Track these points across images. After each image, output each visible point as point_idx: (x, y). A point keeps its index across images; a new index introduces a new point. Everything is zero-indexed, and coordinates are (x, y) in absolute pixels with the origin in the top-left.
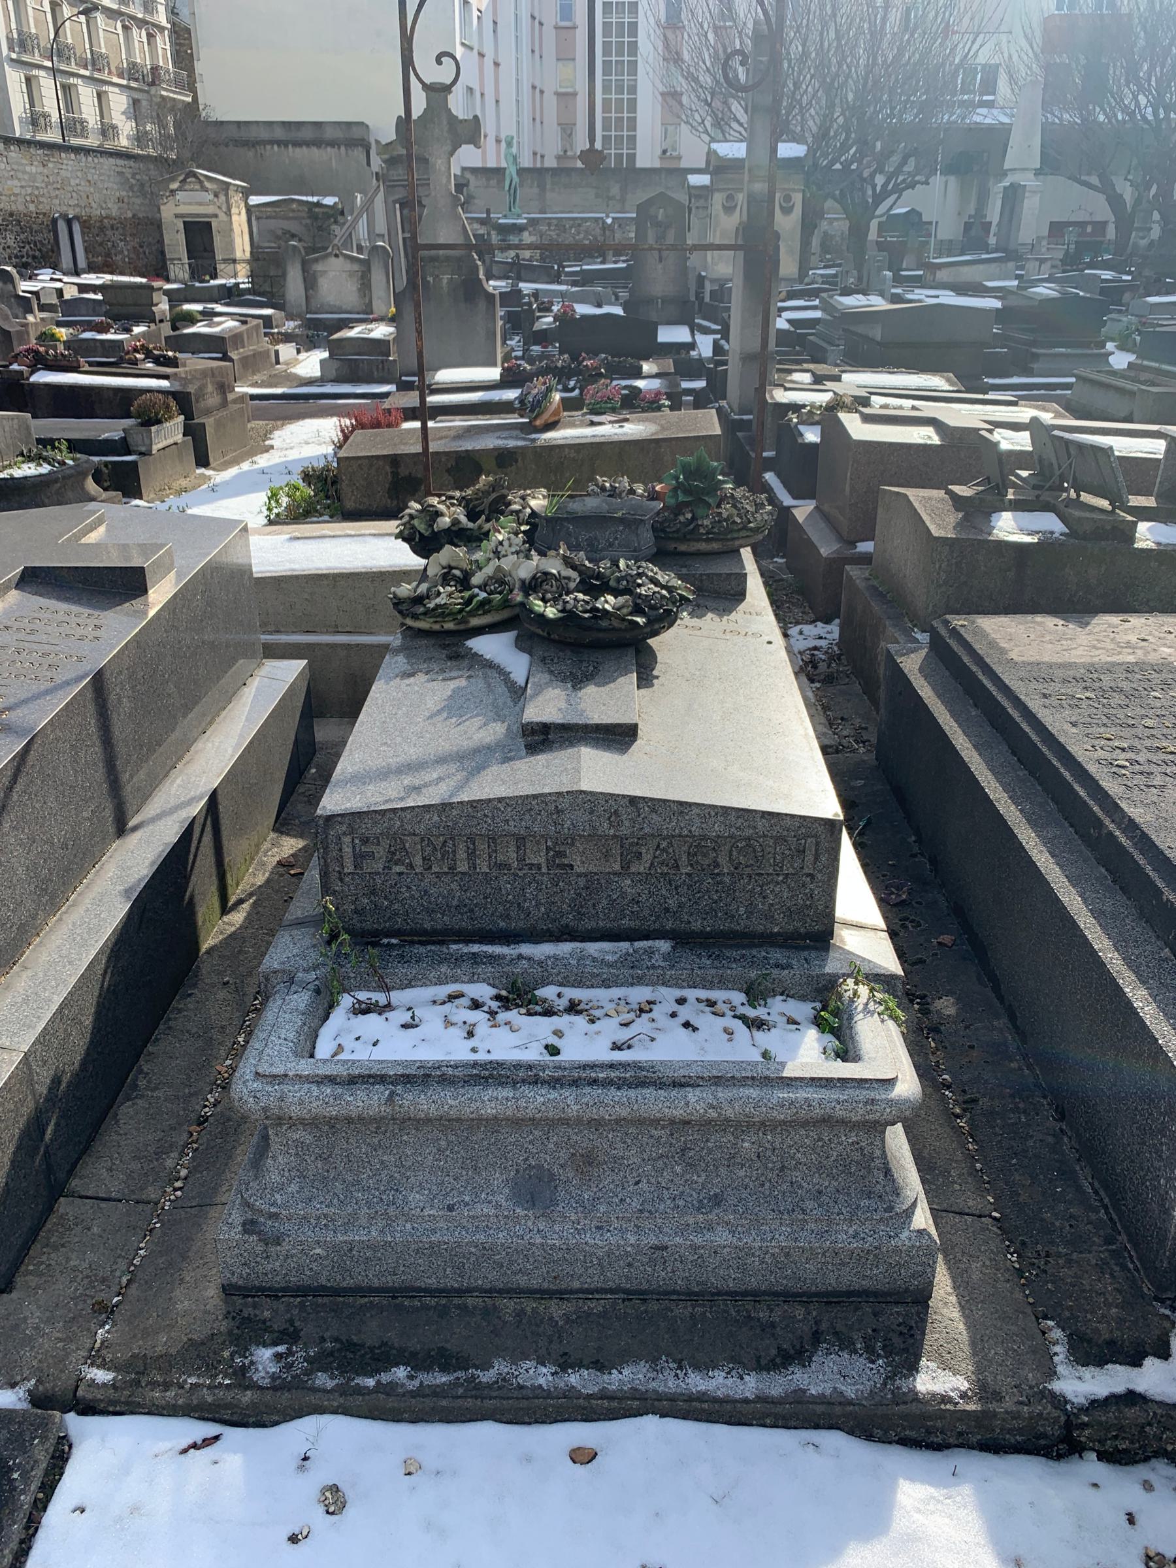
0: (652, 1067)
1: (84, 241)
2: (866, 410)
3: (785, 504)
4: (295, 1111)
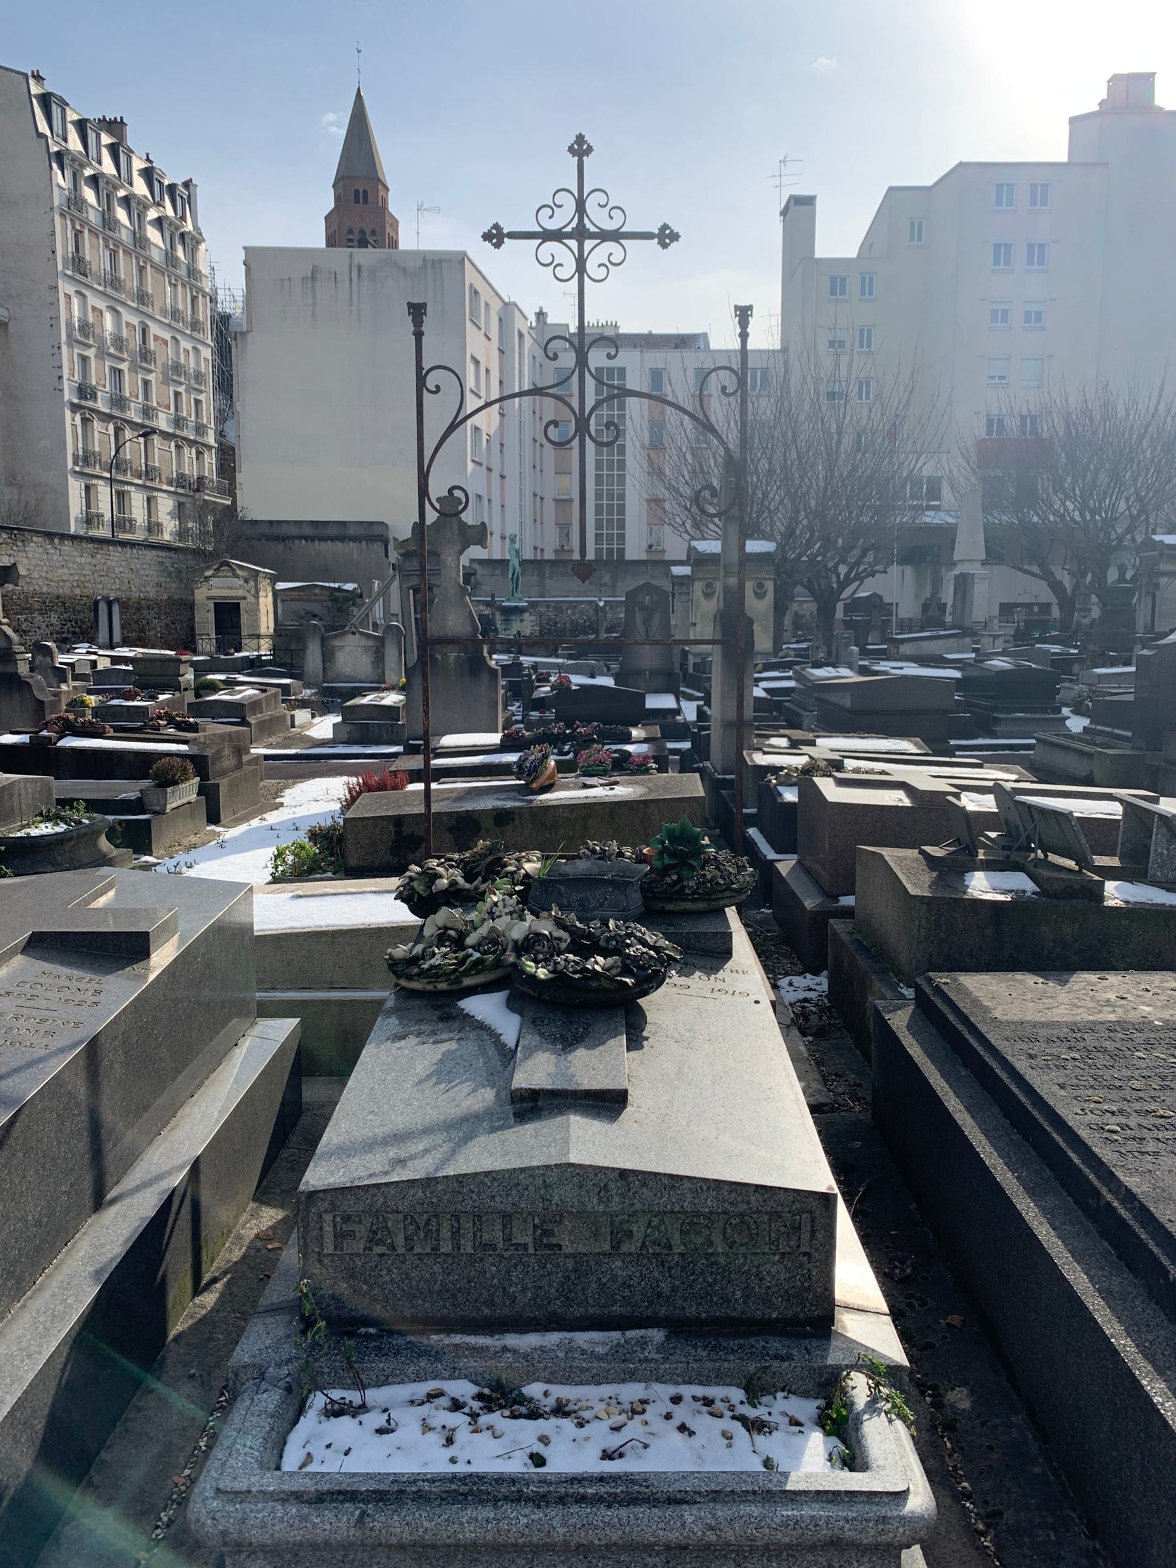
0: (643, 1480)
1: (121, 619)
2: (839, 775)
3: (769, 858)
4: (256, 1536)
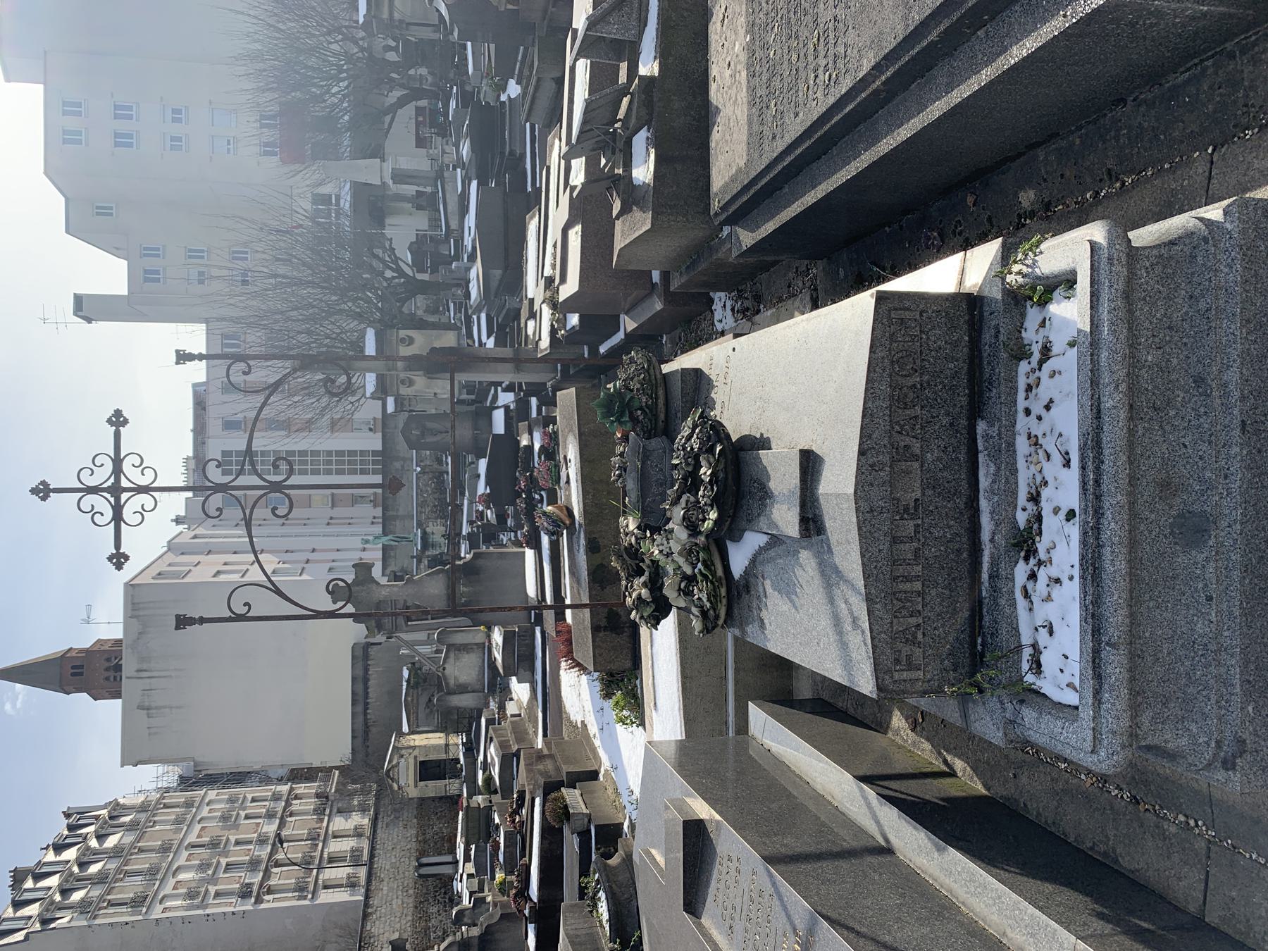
0: (1083, 436)
4: (1125, 723)
